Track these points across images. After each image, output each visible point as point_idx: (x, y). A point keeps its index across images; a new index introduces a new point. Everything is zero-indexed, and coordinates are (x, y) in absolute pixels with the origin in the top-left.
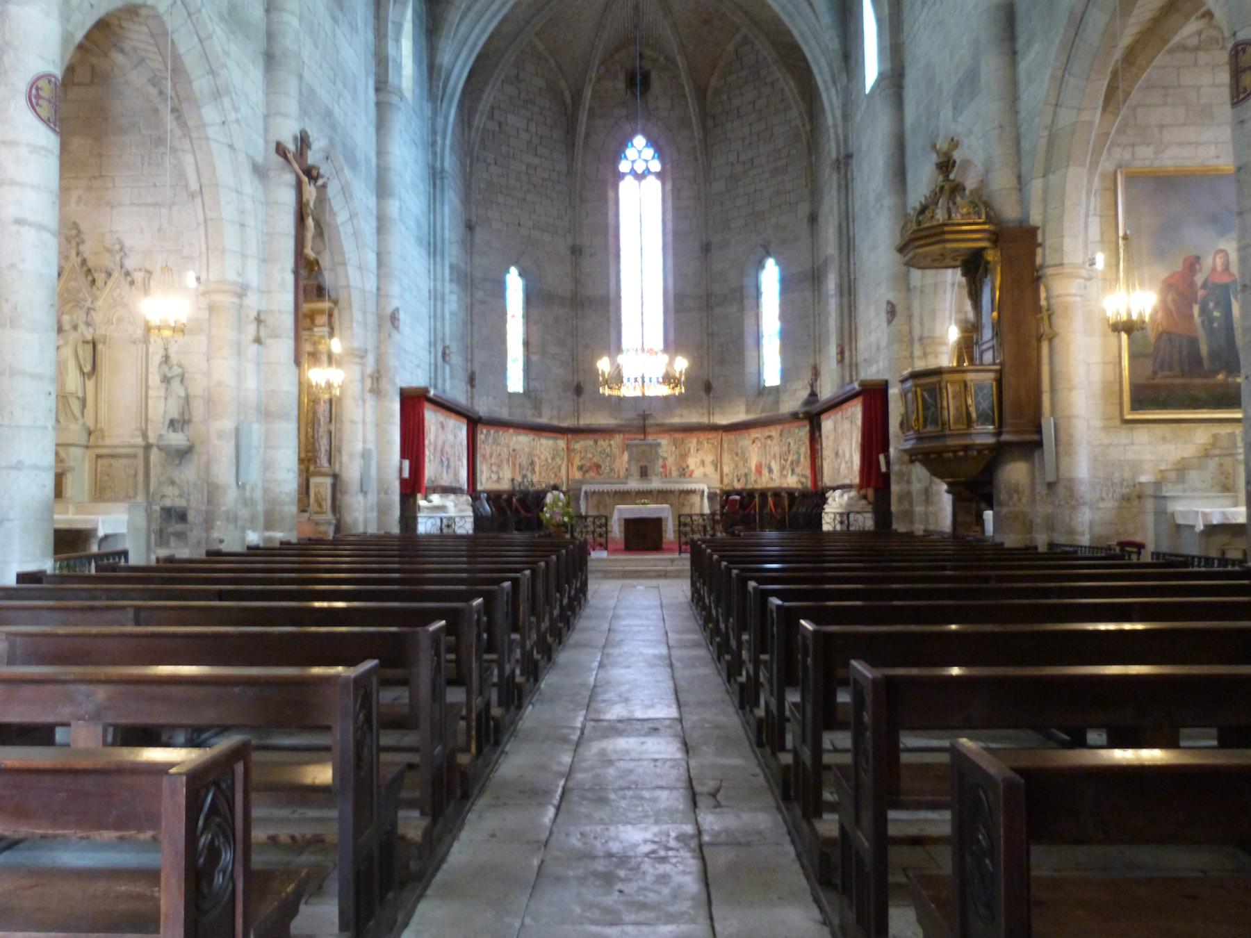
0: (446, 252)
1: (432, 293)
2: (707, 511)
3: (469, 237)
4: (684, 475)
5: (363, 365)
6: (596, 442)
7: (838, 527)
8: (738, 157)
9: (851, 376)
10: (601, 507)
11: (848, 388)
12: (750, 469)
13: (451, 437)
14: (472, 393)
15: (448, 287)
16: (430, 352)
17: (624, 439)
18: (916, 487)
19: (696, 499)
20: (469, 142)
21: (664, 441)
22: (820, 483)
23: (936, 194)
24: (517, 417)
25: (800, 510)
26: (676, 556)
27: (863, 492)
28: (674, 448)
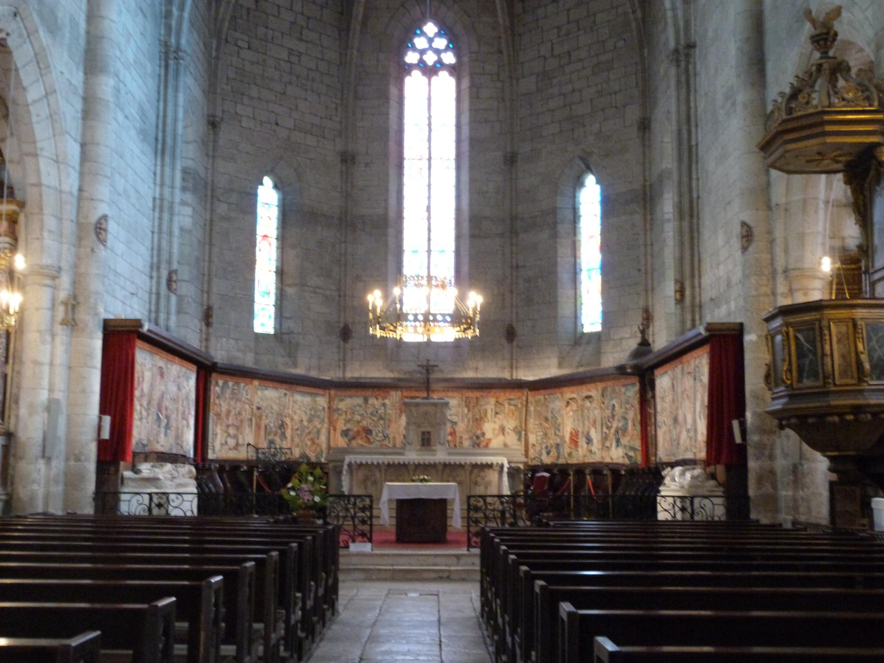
0: (178, 151)
1: (158, 202)
2: (506, 491)
3: (211, 137)
4: (478, 445)
5: (54, 288)
6: (366, 400)
7: (679, 516)
8: (552, 50)
9: (693, 321)
10: (369, 484)
11: (690, 334)
12: (562, 438)
13: (173, 388)
14: (208, 334)
15: (178, 195)
16: (151, 277)
17: (403, 397)
18: (781, 464)
19: (493, 476)
20: (216, 19)
21: (454, 401)
22: (653, 458)
23: (811, 75)
24: (266, 364)
25: (627, 493)
26: (464, 551)
27: (711, 469)
28: (466, 410)
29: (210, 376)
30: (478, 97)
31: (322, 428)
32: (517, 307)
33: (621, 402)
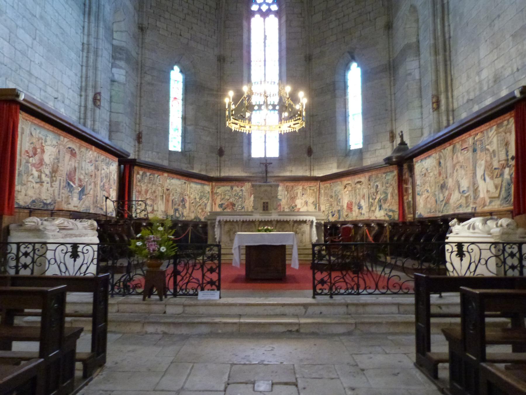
1: (86, 46)
6: (232, 188)
9: (448, 120)
14: (139, 148)
16: (81, 96)
19: (306, 228)
24: (175, 165)
28: (286, 193)
29: (133, 168)
30: (290, 26)
31: (207, 203)
32: (313, 137)
33: (383, 183)
